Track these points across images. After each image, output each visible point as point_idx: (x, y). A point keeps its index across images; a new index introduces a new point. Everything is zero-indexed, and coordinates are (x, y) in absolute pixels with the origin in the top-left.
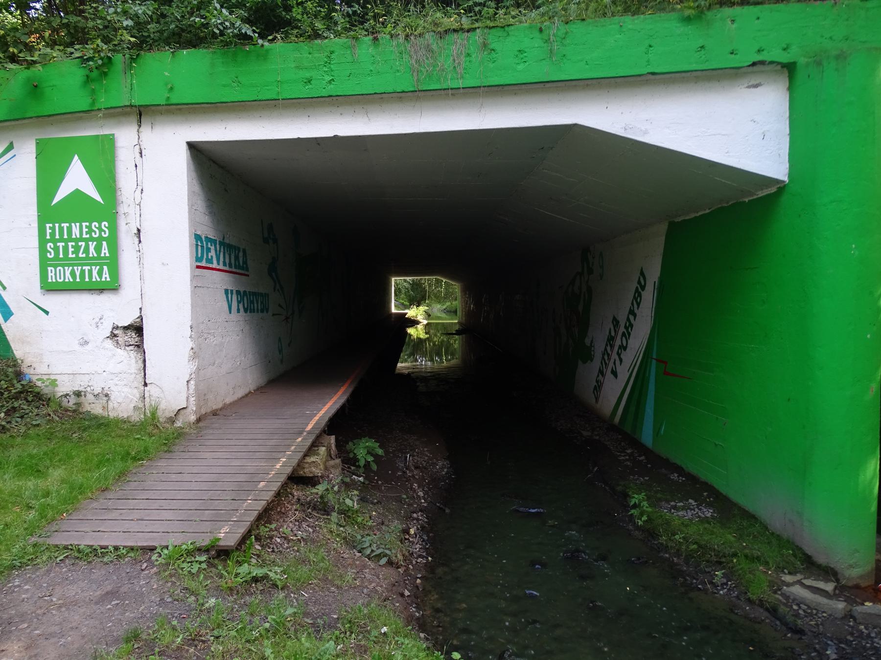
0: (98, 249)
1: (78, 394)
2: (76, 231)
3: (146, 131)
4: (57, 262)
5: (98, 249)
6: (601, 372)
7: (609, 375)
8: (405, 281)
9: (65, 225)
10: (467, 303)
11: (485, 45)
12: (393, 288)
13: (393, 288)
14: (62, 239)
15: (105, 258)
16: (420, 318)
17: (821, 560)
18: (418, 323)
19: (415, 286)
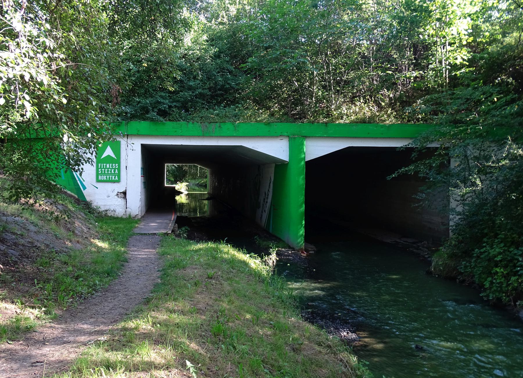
0: (115, 171)
1: (106, 211)
2: (108, 166)
3: (129, 140)
4: (102, 174)
5: (115, 171)
6: (262, 212)
7: (264, 212)
8: (173, 166)
9: (105, 164)
10: (213, 182)
11: (220, 126)
12: (166, 170)
13: (166, 170)
14: (103, 168)
15: (116, 174)
16: (182, 190)
17: (291, 246)
18: (182, 193)
19: (180, 168)
